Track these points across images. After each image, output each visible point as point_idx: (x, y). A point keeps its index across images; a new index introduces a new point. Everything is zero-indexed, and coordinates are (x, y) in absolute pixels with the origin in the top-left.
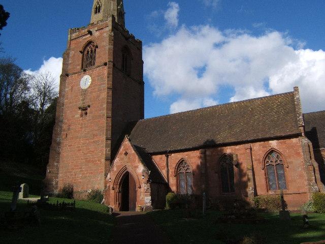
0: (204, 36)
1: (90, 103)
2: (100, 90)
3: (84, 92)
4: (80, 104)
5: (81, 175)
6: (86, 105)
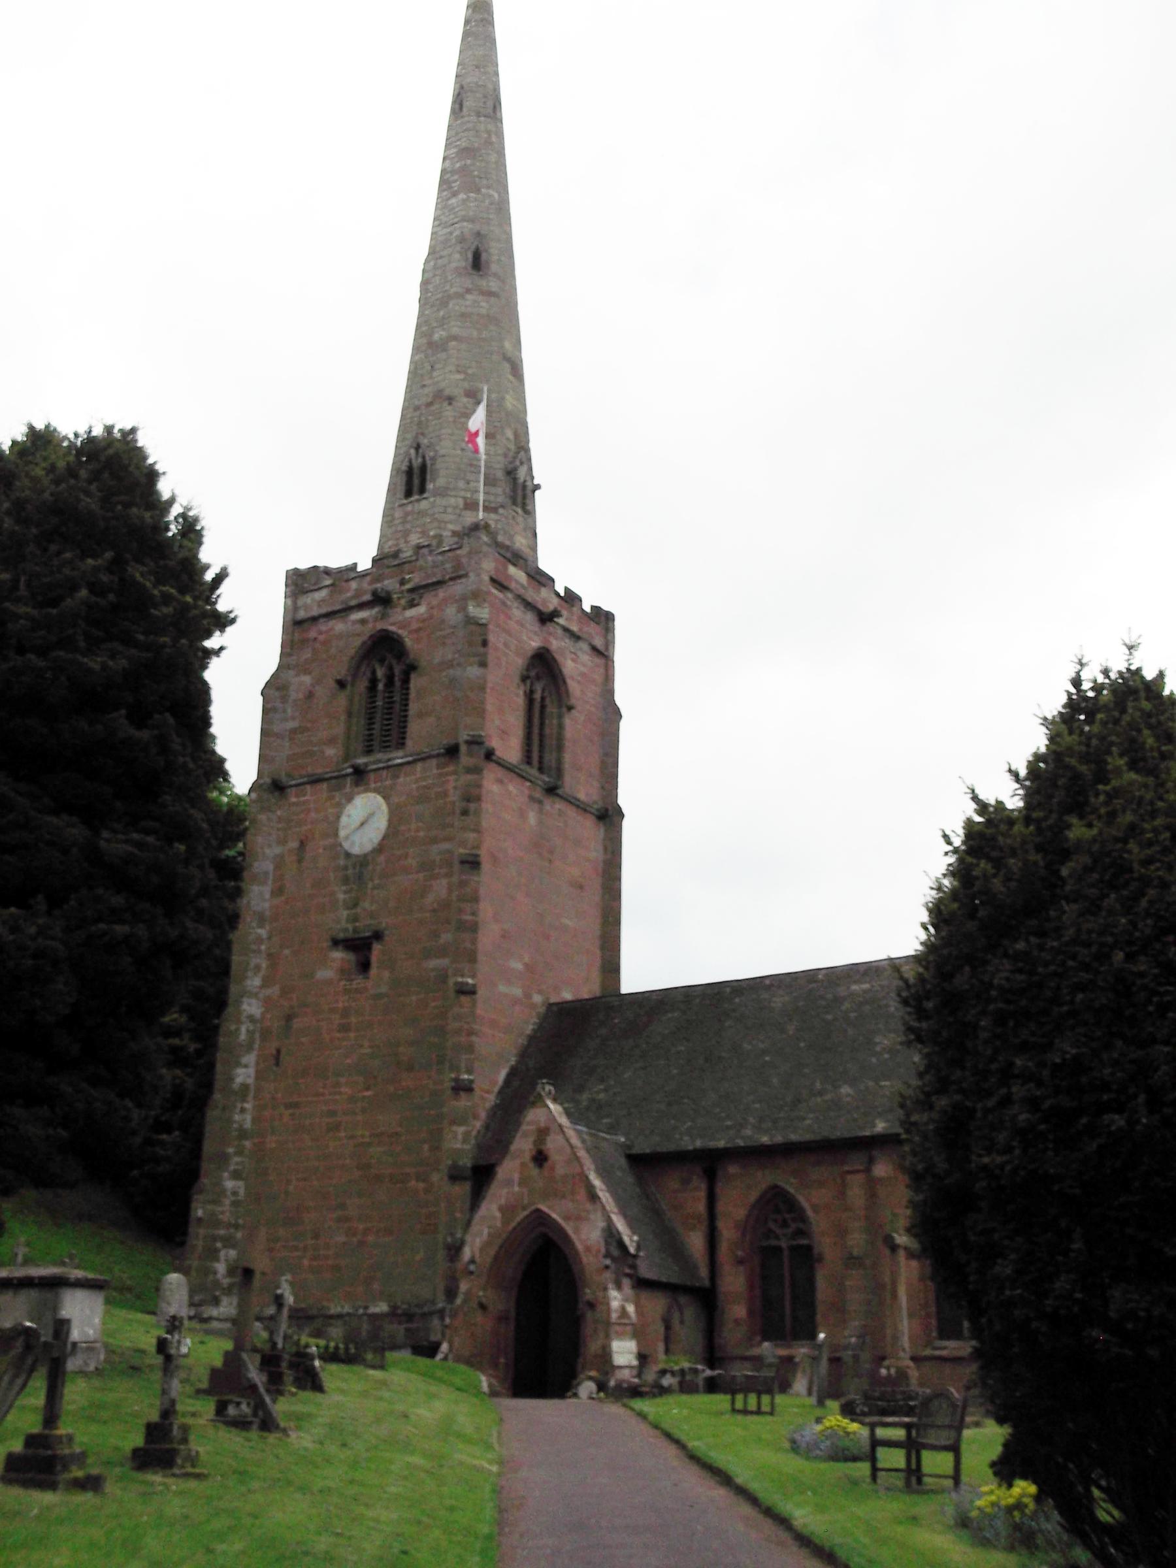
0: (202, 528)
1: (385, 922)
2: (426, 866)
3: (358, 870)
4: (340, 921)
5: (341, 1239)
6: (365, 926)
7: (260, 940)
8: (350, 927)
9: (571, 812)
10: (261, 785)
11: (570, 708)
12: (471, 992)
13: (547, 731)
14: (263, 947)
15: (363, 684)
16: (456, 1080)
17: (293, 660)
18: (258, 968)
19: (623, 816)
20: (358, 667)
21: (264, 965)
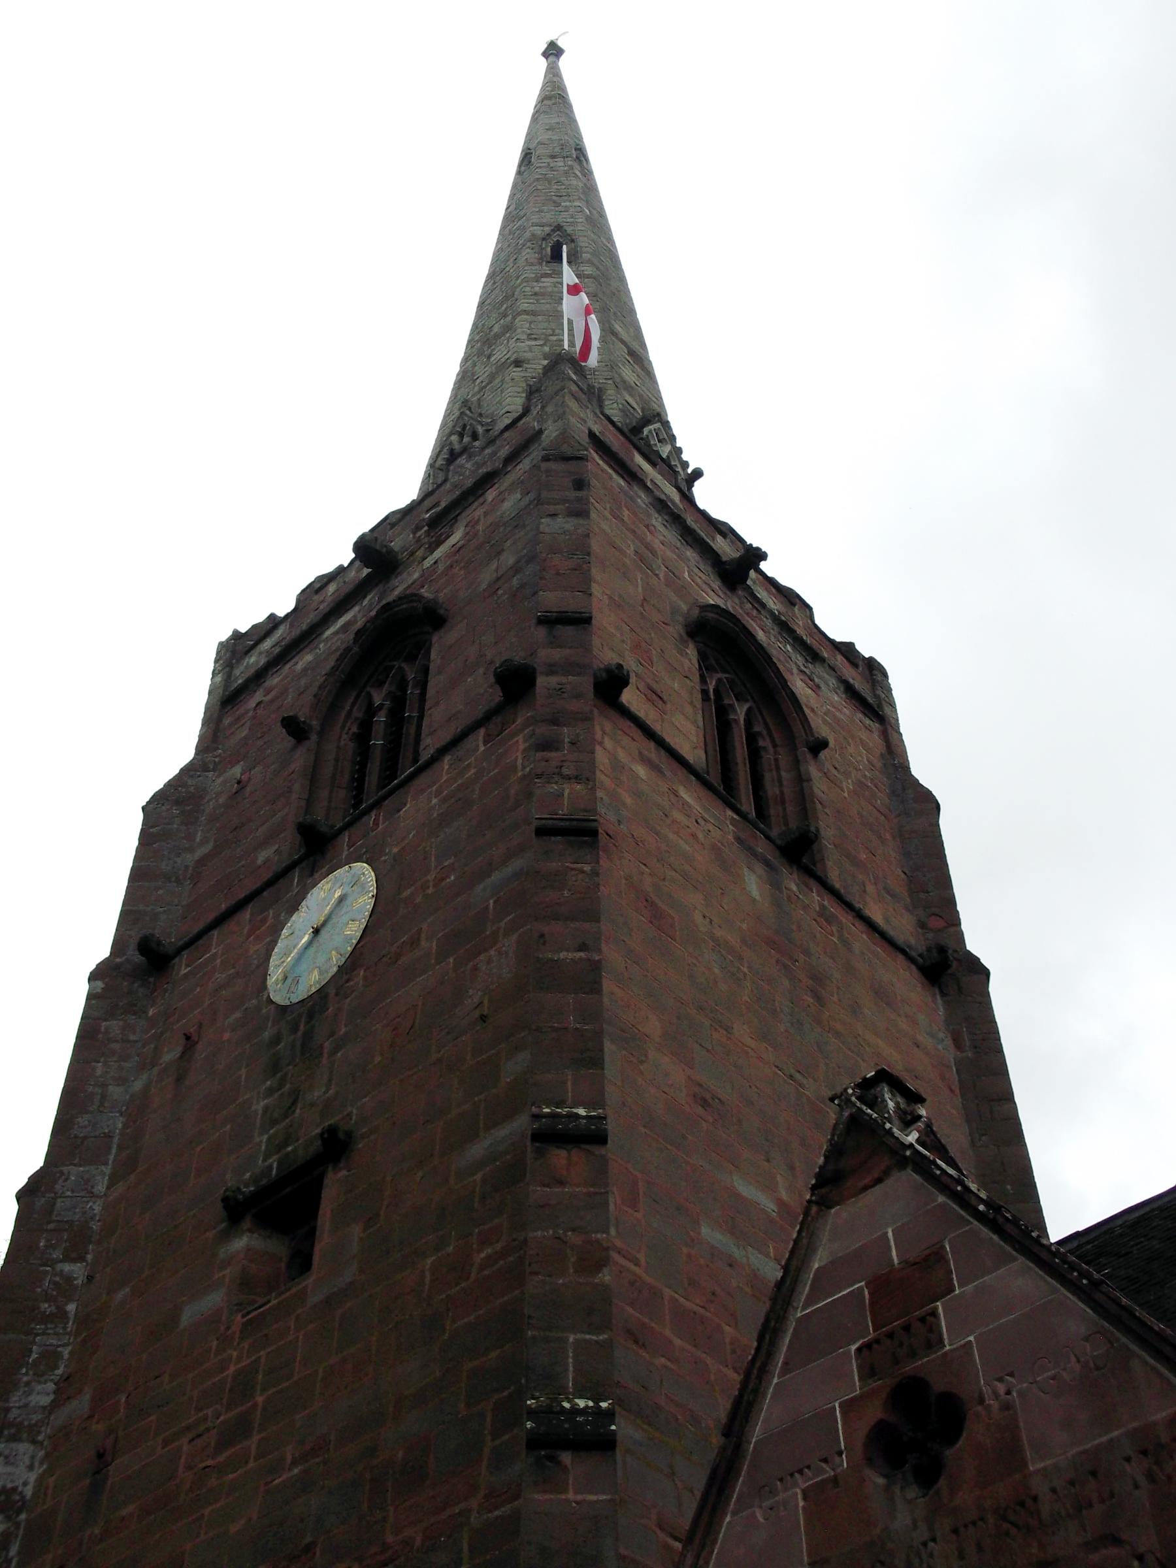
7: (66, 1288)
8: (273, 1161)
9: (860, 938)
10: (118, 967)
11: (818, 746)
12: (592, 1136)
13: (771, 789)
14: (71, 1307)
15: (342, 738)
16: (548, 1412)
17: (209, 757)
18: (51, 1358)
19: (986, 973)
20: (334, 707)
21: (66, 1352)
